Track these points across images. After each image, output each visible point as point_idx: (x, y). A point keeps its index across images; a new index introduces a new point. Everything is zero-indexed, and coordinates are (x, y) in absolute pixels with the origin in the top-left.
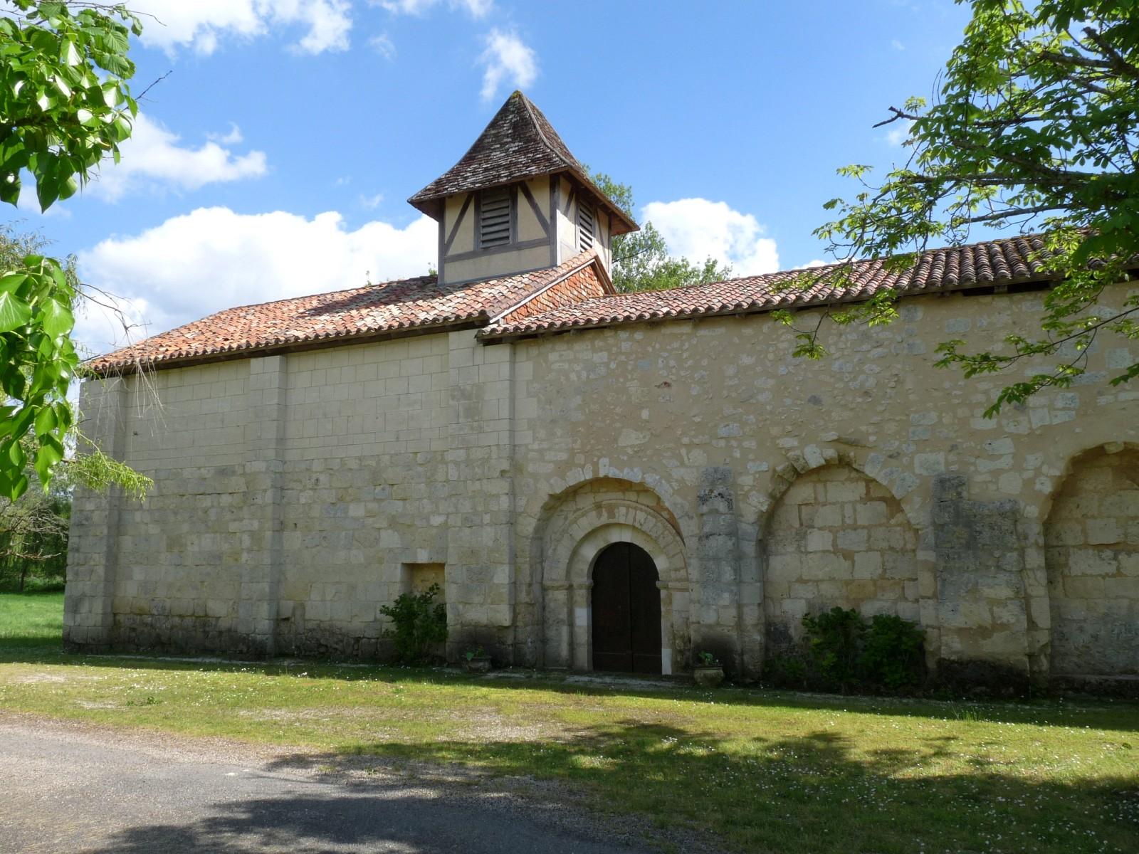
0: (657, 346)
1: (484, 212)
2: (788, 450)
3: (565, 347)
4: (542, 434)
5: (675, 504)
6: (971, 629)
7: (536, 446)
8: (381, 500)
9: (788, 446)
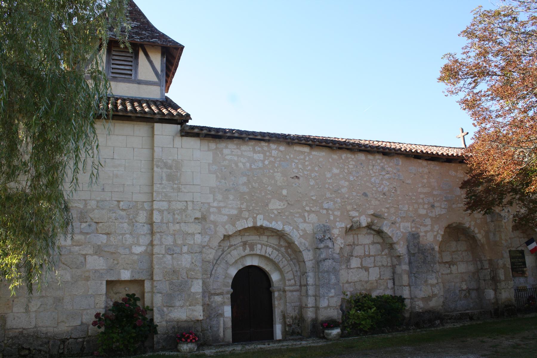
0: (292, 156)
1: (114, 55)
2: (354, 217)
3: (235, 147)
4: (219, 197)
5: (301, 243)
6: (426, 297)
7: (215, 204)
8: (87, 233)
9: (354, 215)
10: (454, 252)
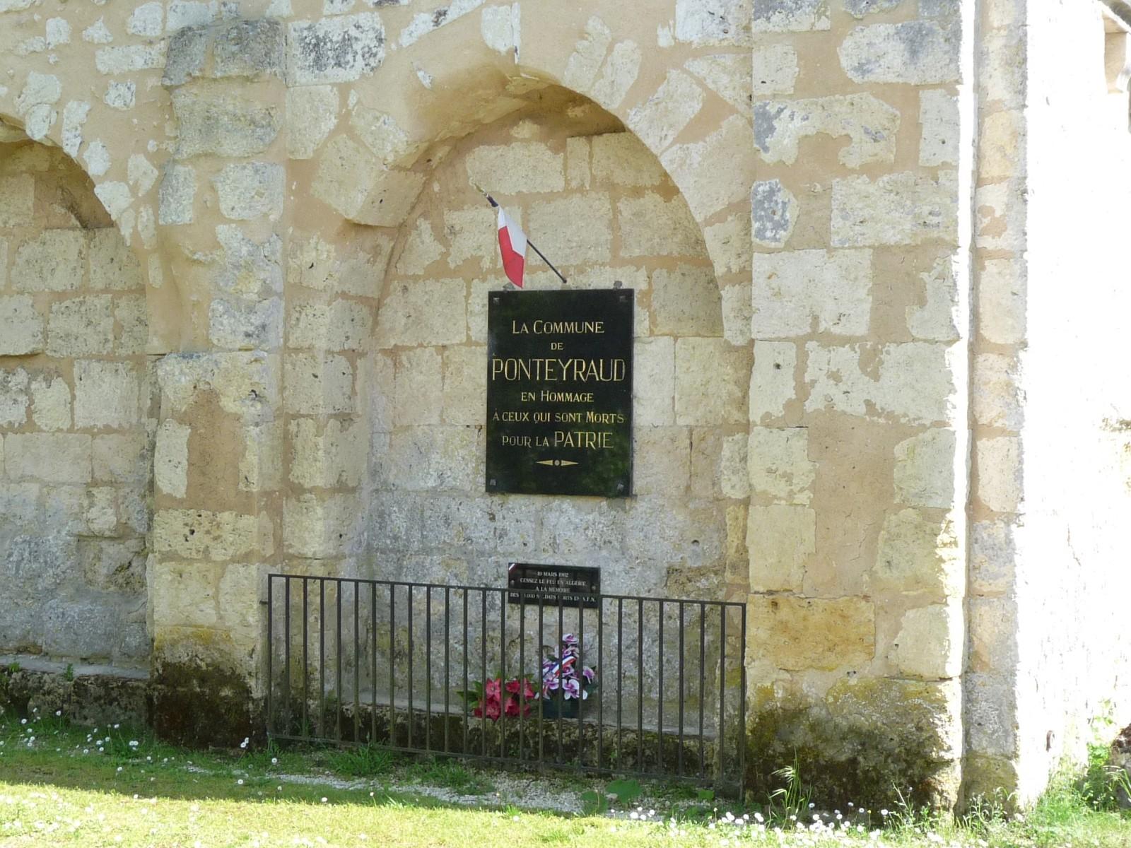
10: (60, 296)
